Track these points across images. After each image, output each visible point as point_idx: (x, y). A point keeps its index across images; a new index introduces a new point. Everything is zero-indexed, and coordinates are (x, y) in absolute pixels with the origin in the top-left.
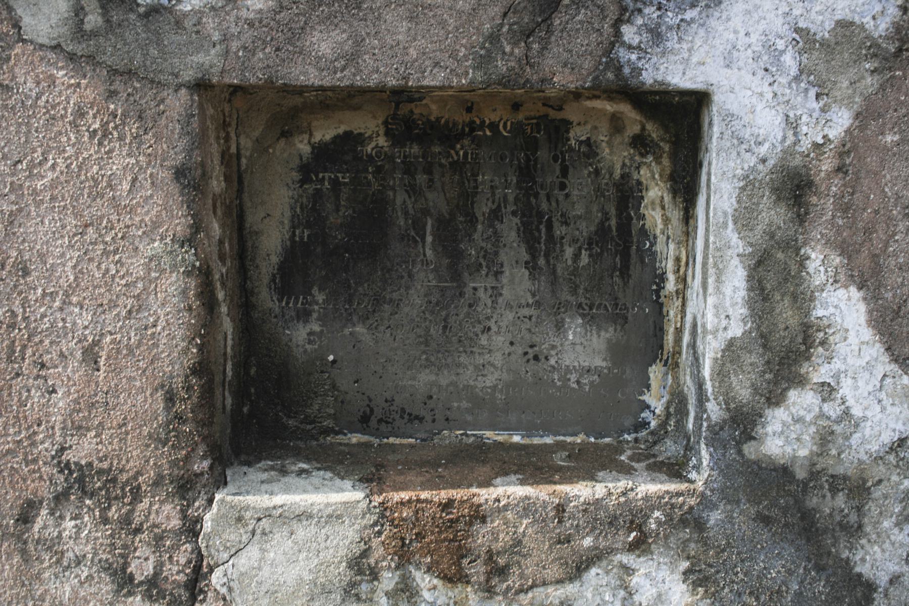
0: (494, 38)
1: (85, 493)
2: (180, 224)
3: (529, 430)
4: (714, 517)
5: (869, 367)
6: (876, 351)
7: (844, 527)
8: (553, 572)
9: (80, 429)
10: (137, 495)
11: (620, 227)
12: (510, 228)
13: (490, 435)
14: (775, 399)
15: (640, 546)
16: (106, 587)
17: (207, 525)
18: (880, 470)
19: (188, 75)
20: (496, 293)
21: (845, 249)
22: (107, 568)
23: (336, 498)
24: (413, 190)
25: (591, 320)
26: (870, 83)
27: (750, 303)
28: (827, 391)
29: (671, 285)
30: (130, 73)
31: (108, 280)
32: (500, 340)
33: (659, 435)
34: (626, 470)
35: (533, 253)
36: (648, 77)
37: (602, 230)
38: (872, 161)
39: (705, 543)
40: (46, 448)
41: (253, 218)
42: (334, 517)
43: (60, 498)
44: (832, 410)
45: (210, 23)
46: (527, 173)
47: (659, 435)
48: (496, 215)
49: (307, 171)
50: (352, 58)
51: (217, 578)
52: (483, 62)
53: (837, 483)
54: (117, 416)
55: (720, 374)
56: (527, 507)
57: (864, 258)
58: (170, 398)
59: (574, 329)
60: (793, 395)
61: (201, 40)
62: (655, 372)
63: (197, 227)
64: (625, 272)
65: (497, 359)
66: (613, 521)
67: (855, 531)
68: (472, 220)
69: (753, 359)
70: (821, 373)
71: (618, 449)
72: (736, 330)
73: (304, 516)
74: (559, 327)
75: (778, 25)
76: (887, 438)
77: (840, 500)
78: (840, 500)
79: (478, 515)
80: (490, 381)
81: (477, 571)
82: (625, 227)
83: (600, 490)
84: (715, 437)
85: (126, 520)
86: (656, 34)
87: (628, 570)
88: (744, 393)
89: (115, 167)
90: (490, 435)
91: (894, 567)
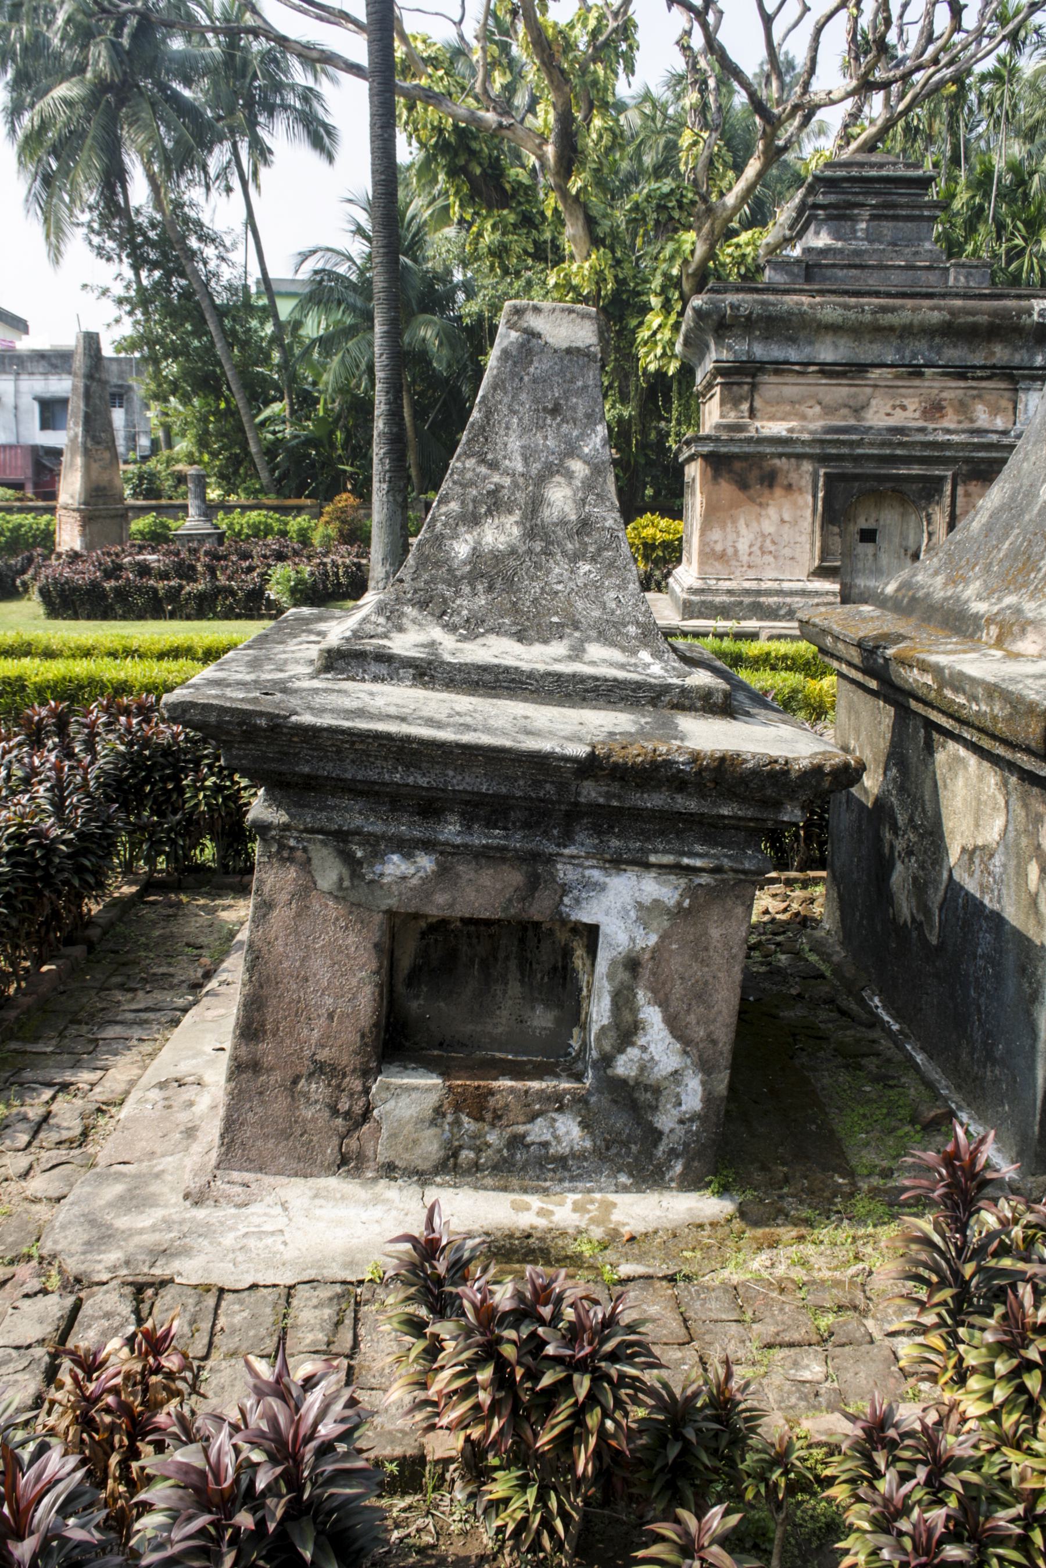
0: (510, 900)
1: (322, 1073)
2: (374, 965)
3: (516, 1054)
4: (593, 1099)
5: (663, 1040)
6: (665, 1033)
7: (650, 1107)
8: (521, 1119)
9: (323, 1046)
10: (344, 1076)
11: (636, 814)
12: (513, 965)
13: (498, 1055)
14: (621, 1050)
15: (560, 1110)
16: (327, 1114)
17: (374, 1090)
18: (666, 1083)
19: (384, 908)
20: (505, 992)
21: (654, 991)
22: (328, 1105)
23: (430, 1082)
24: (470, 945)
25: (548, 1007)
26: (666, 924)
27: (612, 1011)
28: (644, 1049)
29: (585, 993)
30: (359, 905)
31: (342, 987)
32: (505, 1013)
33: (576, 1059)
34: (557, 1076)
35: (523, 974)
36: (573, 918)
37: (555, 968)
38: (666, 955)
39: (588, 1110)
40: (307, 1053)
41: (397, 954)
42: (428, 1090)
43: (311, 1075)
44: (646, 1057)
45: (394, 888)
46: (522, 941)
47: (576, 1059)
48: (507, 958)
49: (423, 934)
50: (451, 906)
51: (375, 1113)
52: (505, 909)
53: (647, 1088)
54: (339, 1042)
55: (598, 1039)
56: (512, 1090)
57: (661, 994)
58: (363, 1036)
59: (539, 1010)
60: (629, 1050)
61: (390, 894)
62: (576, 1031)
63: (380, 967)
64: (564, 986)
65: (504, 1021)
66: (549, 1098)
67: (655, 1109)
68: (496, 959)
69: (612, 1034)
70: (642, 1041)
71: (557, 1064)
72: (605, 1022)
73: (415, 1088)
74: (533, 1008)
75: (628, 900)
76: (670, 1069)
77: (649, 1095)
78: (649, 1095)
79: (491, 1093)
80: (500, 1030)
81: (489, 1116)
82: (565, 968)
83: (544, 1085)
84: (595, 1065)
85: (339, 1086)
86: (577, 901)
87: (554, 1120)
88: (607, 1047)
89: (349, 941)
90: (498, 1055)
91: (672, 1125)
